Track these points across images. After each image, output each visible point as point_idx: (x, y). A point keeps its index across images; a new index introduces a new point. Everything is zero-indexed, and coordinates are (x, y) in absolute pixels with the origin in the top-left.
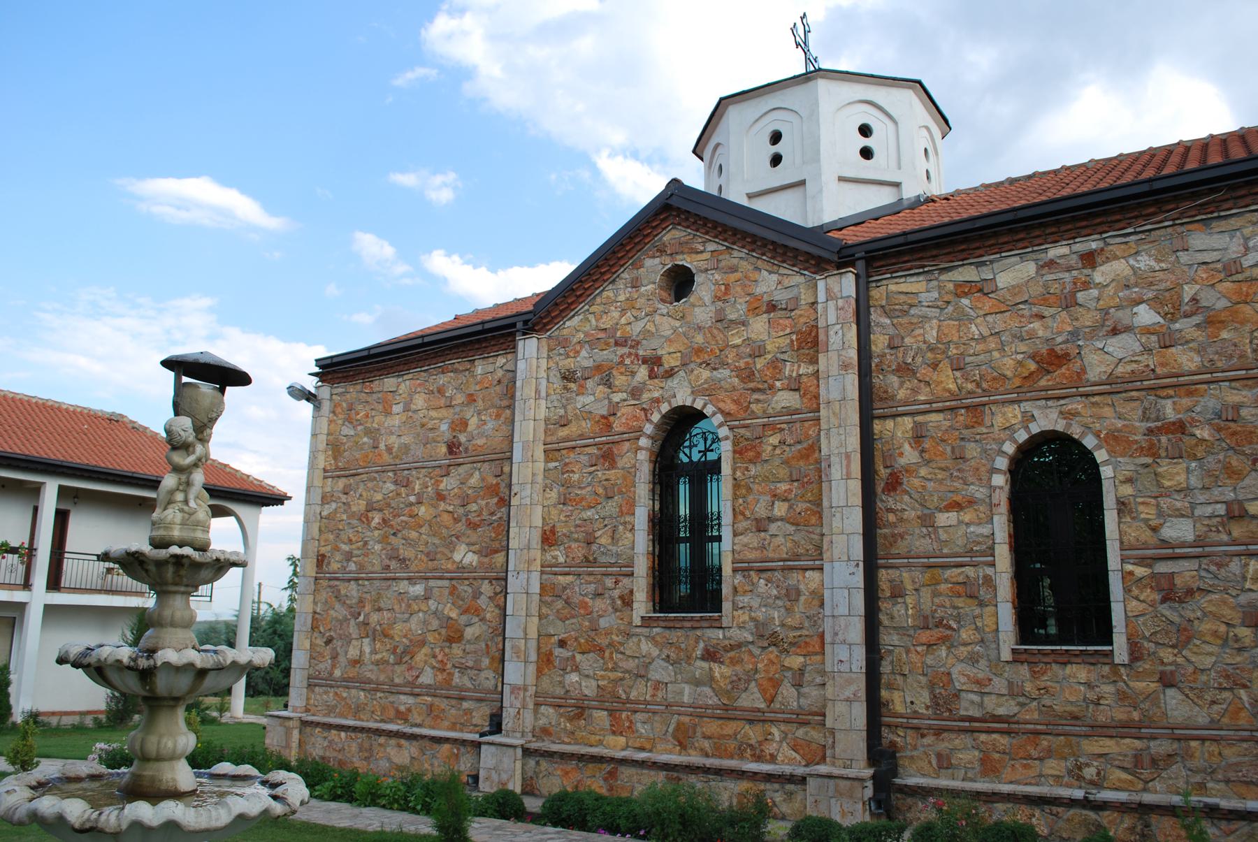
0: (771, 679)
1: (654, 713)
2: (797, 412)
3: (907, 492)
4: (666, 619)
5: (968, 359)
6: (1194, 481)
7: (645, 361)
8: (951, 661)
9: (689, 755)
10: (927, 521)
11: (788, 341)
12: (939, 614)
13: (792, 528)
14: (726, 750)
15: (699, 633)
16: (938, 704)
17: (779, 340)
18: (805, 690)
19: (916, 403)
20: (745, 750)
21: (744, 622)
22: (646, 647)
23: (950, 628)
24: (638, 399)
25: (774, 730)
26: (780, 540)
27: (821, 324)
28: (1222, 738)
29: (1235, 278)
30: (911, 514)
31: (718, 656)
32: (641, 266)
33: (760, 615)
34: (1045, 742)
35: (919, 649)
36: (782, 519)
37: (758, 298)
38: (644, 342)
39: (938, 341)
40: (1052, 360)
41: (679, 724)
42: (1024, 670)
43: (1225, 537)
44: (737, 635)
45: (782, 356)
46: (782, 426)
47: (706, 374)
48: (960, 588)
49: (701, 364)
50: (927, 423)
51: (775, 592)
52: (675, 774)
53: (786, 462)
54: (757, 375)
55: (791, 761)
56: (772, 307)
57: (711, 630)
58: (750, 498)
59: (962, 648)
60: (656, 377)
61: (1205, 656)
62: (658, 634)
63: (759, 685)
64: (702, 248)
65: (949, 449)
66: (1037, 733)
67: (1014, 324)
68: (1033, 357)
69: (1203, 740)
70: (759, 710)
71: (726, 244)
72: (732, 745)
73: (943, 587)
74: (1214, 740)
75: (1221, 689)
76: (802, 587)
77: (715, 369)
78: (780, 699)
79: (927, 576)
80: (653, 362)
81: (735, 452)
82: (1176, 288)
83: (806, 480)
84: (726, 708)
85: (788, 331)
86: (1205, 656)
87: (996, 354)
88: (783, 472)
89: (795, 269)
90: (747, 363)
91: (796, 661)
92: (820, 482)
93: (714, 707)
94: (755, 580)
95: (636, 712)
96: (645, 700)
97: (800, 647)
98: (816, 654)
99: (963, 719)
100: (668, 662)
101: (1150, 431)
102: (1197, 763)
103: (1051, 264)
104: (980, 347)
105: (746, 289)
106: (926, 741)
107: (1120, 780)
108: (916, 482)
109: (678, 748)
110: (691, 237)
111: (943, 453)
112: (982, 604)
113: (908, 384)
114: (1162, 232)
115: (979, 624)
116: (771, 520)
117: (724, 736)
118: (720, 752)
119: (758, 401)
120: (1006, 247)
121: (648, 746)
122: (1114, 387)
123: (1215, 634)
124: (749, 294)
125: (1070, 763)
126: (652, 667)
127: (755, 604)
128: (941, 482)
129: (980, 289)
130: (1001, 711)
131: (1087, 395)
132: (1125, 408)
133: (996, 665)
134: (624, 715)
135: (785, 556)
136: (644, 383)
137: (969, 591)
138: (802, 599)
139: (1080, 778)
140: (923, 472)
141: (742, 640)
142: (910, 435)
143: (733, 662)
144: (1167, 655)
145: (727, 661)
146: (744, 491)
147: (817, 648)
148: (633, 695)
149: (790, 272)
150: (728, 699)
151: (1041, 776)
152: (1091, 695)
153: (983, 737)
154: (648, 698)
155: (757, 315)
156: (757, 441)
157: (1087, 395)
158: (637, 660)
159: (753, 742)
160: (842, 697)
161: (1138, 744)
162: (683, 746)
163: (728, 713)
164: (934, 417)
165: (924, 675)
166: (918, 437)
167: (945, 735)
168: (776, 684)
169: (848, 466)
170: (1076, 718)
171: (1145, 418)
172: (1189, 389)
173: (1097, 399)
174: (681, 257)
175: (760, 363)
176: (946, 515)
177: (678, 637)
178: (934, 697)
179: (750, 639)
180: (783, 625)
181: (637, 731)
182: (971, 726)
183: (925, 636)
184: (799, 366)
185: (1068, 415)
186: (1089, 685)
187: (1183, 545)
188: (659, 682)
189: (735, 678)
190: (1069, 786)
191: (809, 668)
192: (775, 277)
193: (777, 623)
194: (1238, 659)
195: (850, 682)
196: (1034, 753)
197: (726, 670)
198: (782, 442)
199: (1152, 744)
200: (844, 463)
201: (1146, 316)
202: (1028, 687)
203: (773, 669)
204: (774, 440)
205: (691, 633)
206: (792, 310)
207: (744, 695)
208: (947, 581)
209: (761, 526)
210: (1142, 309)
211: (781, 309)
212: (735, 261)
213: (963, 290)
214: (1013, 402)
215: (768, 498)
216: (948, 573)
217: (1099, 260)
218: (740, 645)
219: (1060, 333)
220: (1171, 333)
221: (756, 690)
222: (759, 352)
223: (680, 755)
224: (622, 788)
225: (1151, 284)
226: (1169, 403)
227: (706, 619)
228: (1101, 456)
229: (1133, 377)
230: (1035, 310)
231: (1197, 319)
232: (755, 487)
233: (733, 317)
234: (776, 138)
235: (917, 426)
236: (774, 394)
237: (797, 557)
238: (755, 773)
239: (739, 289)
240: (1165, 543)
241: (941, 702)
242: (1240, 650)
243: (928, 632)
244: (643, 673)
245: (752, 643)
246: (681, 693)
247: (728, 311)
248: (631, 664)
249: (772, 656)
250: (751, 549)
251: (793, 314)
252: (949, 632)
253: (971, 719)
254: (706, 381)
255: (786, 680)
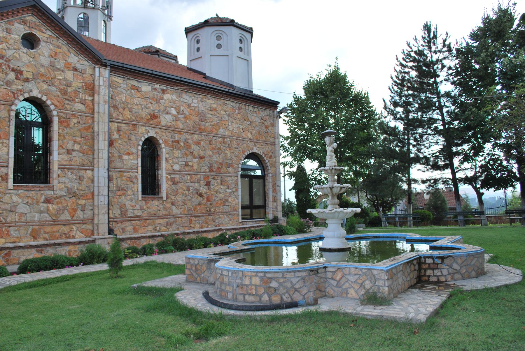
0: (73, 209)
1: (20, 226)
2: (83, 112)
3: (115, 147)
4: (26, 187)
5: (134, 110)
6: (180, 156)
7: (13, 70)
8: (125, 200)
9: (39, 241)
10: (120, 157)
11: (81, 85)
12: (123, 186)
13: (82, 155)
14: (55, 236)
15: (42, 192)
16: (122, 214)
17: (78, 83)
18: (86, 212)
19: (118, 119)
20: (62, 236)
21: (62, 188)
22: (15, 198)
23: (126, 190)
24: (9, 87)
25: (74, 227)
26: (77, 158)
27: (96, 83)
28: (182, 217)
29: (190, 108)
30: (116, 155)
31: (51, 201)
32: (13, 25)
33: (69, 185)
34: (148, 222)
35: (117, 197)
36: (77, 151)
37: (69, 64)
38: (12, 61)
39: (125, 101)
40: (154, 117)
41: (33, 230)
42: (144, 202)
43: (184, 170)
44: (59, 193)
45: (79, 90)
46: (79, 116)
47: (45, 86)
48: (128, 179)
49: (43, 81)
50: (121, 126)
51: (75, 177)
52: (40, 249)
53: (80, 130)
54: (68, 94)
55: (81, 237)
56: (75, 70)
57: (48, 191)
58: (65, 141)
59: (128, 197)
60: (20, 80)
61: (180, 198)
62: (21, 193)
63: (69, 211)
64: (45, 32)
65: (127, 136)
66: (146, 219)
67: (145, 103)
68: (150, 114)
69: (179, 217)
70: (68, 220)
71: (57, 35)
72: (58, 235)
73: (124, 178)
74: (181, 217)
75: (182, 205)
76: (85, 176)
77: (50, 86)
78: (76, 216)
79: (119, 174)
80: (18, 73)
81: (59, 122)
82: (179, 106)
83: (87, 138)
84: (54, 221)
85: (81, 81)
86: (180, 198)
87: (140, 111)
88: (78, 134)
89: (86, 59)
90: (64, 88)
91: (82, 202)
92: (93, 139)
93: (49, 221)
94: (67, 172)
95: (10, 227)
96: (15, 221)
97: (84, 197)
98: (90, 199)
99: (129, 217)
100: (27, 204)
101: (172, 141)
102: (178, 223)
103: (155, 89)
104: (136, 107)
105: (65, 58)
106: (119, 225)
107: (164, 229)
108: (118, 144)
109: (33, 239)
110: (40, 24)
111: (125, 137)
112: (134, 184)
113: (116, 112)
114: (178, 91)
115: (133, 189)
116: (73, 150)
117: (54, 232)
118: (52, 237)
119: (68, 104)
120: (146, 79)
121: (18, 241)
122: (167, 128)
123: (182, 192)
124: (65, 60)
125: (153, 227)
126: (18, 207)
127: (67, 181)
128: (124, 146)
129: (138, 89)
130: (139, 214)
131: (160, 129)
132: (168, 134)
133: (137, 201)
134: (4, 229)
135: (78, 164)
136: (13, 81)
137: (130, 180)
138: (85, 180)
139: (156, 230)
140: (120, 142)
141: (62, 194)
142: (116, 129)
143: (57, 203)
144: (173, 197)
145: (55, 203)
146: (62, 138)
147: (91, 197)
148: (9, 220)
149: (83, 59)
150: (56, 217)
151: (147, 231)
152: (159, 208)
153: (133, 222)
154: (17, 220)
155: (69, 70)
156: (69, 120)
157: (160, 129)
158: (10, 205)
159: (66, 232)
160: (102, 213)
161: (167, 220)
162: (35, 238)
163: (55, 222)
164: (123, 125)
165: (118, 205)
166: (119, 130)
167: (124, 222)
168: (75, 210)
169: (105, 136)
170: (155, 215)
171: (172, 138)
172: (180, 133)
173: (162, 130)
174: (35, 30)
175: (69, 90)
176: (125, 156)
177: (32, 194)
178: (121, 211)
179: (65, 194)
180: (78, 189)
181: (11, 235)
182: (131, 219)
183: (119, 193)
184: (85, 96)
185: (156, 133)
186: (158, 206)
187: (177, 171)
188: (22, 213)
189: (58, 209)
190: (153, 232)
191: (87, 204)
192: (77, 58)
193: (76, 188)
194: (185, 198)
195: (104, 208)
196: (146, 225)
197: (55, 206)
198: (78, 122)
199: (170, 219)
200: (104, 135)
201: (174, 112)
202: (145, 207)
203: (73, 205)
204: (75, 121)
205: (39, 192)
206: (83, 74)
207: (62, 215)
208: (125, 176)
209: (69, 152)
210: (173, 109)
211: (79, 72)
212: (60, 44)
213: (133, 87)
214: (144, 126)
215: (72, 142)
216: (125, 174)
217: (166, 92)
218: (61, 197)
219: (156, 109)
220: (178, 117)
221: (67, 213)
222: (69, 85)
223: (34, 241)
224: (13, 259)
225: (175, 103)
226: (176, 135)
227: (46, 187)
228: (163, 146)
229: (170, 127)
230: (150, 101)
231: (183, 116)
232: (67, 137)
233: (58, 67)
234: (198, 50)
235: (118, 127)
236: (75, 103)
237: (83, 165)
238: (75, 242)
239: (61, 56)
240: (174, 170)
241: (123, 213)
242: (185, 196)
243: (119, 192)
244: (14, 210)
245: (66, 196)
246: (34, 217)
247: (56, 63)
248: (7, 207)
249: (74, 201)
250: (65, 160)
251: (83, 75)
252: (125, 192)
253: (131, 217)
254: (45, 90)
255: (79, 209)
